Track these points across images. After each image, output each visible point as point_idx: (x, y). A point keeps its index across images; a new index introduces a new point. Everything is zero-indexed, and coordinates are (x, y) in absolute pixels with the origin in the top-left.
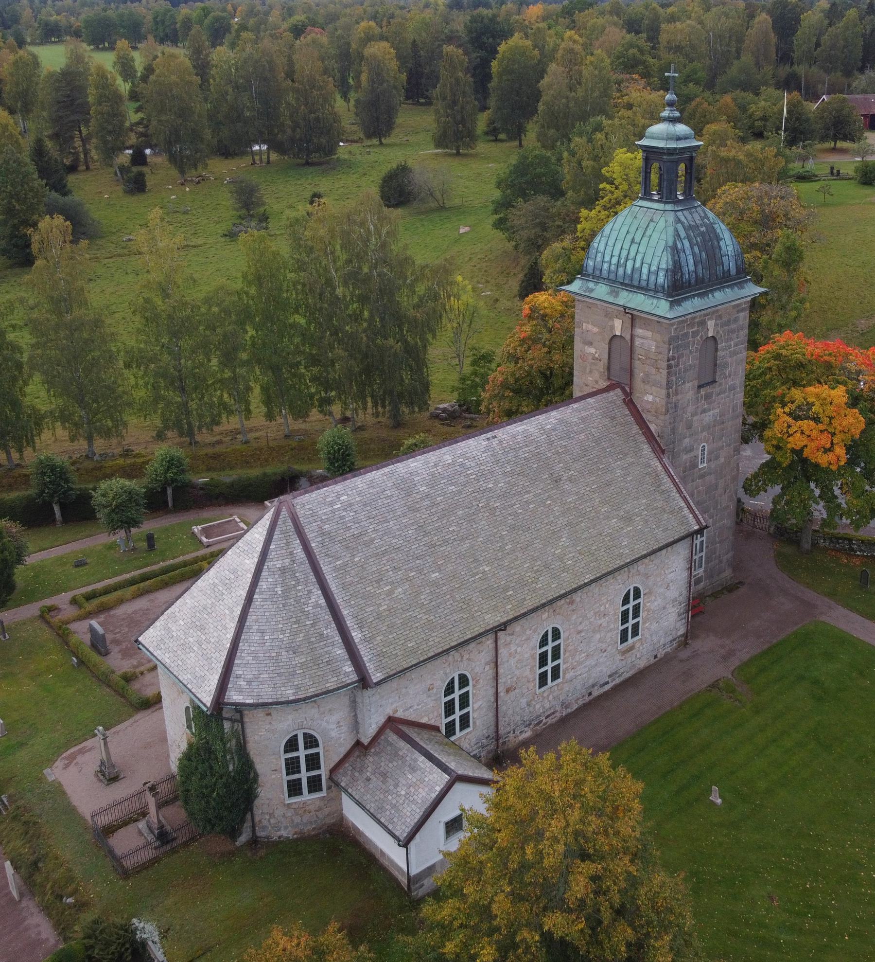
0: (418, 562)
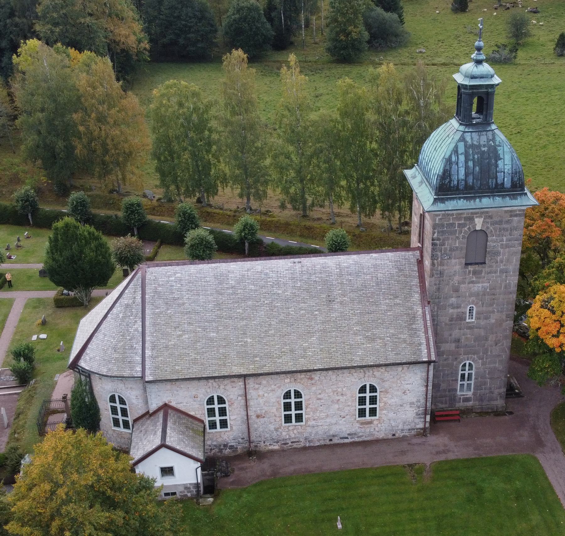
0: (206, 324)
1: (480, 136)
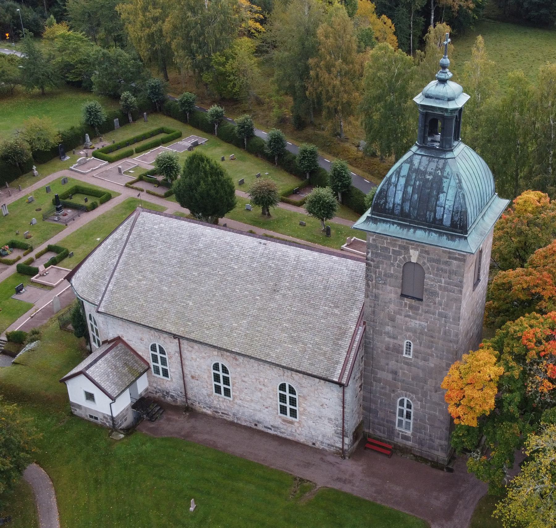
1: (429, 162)
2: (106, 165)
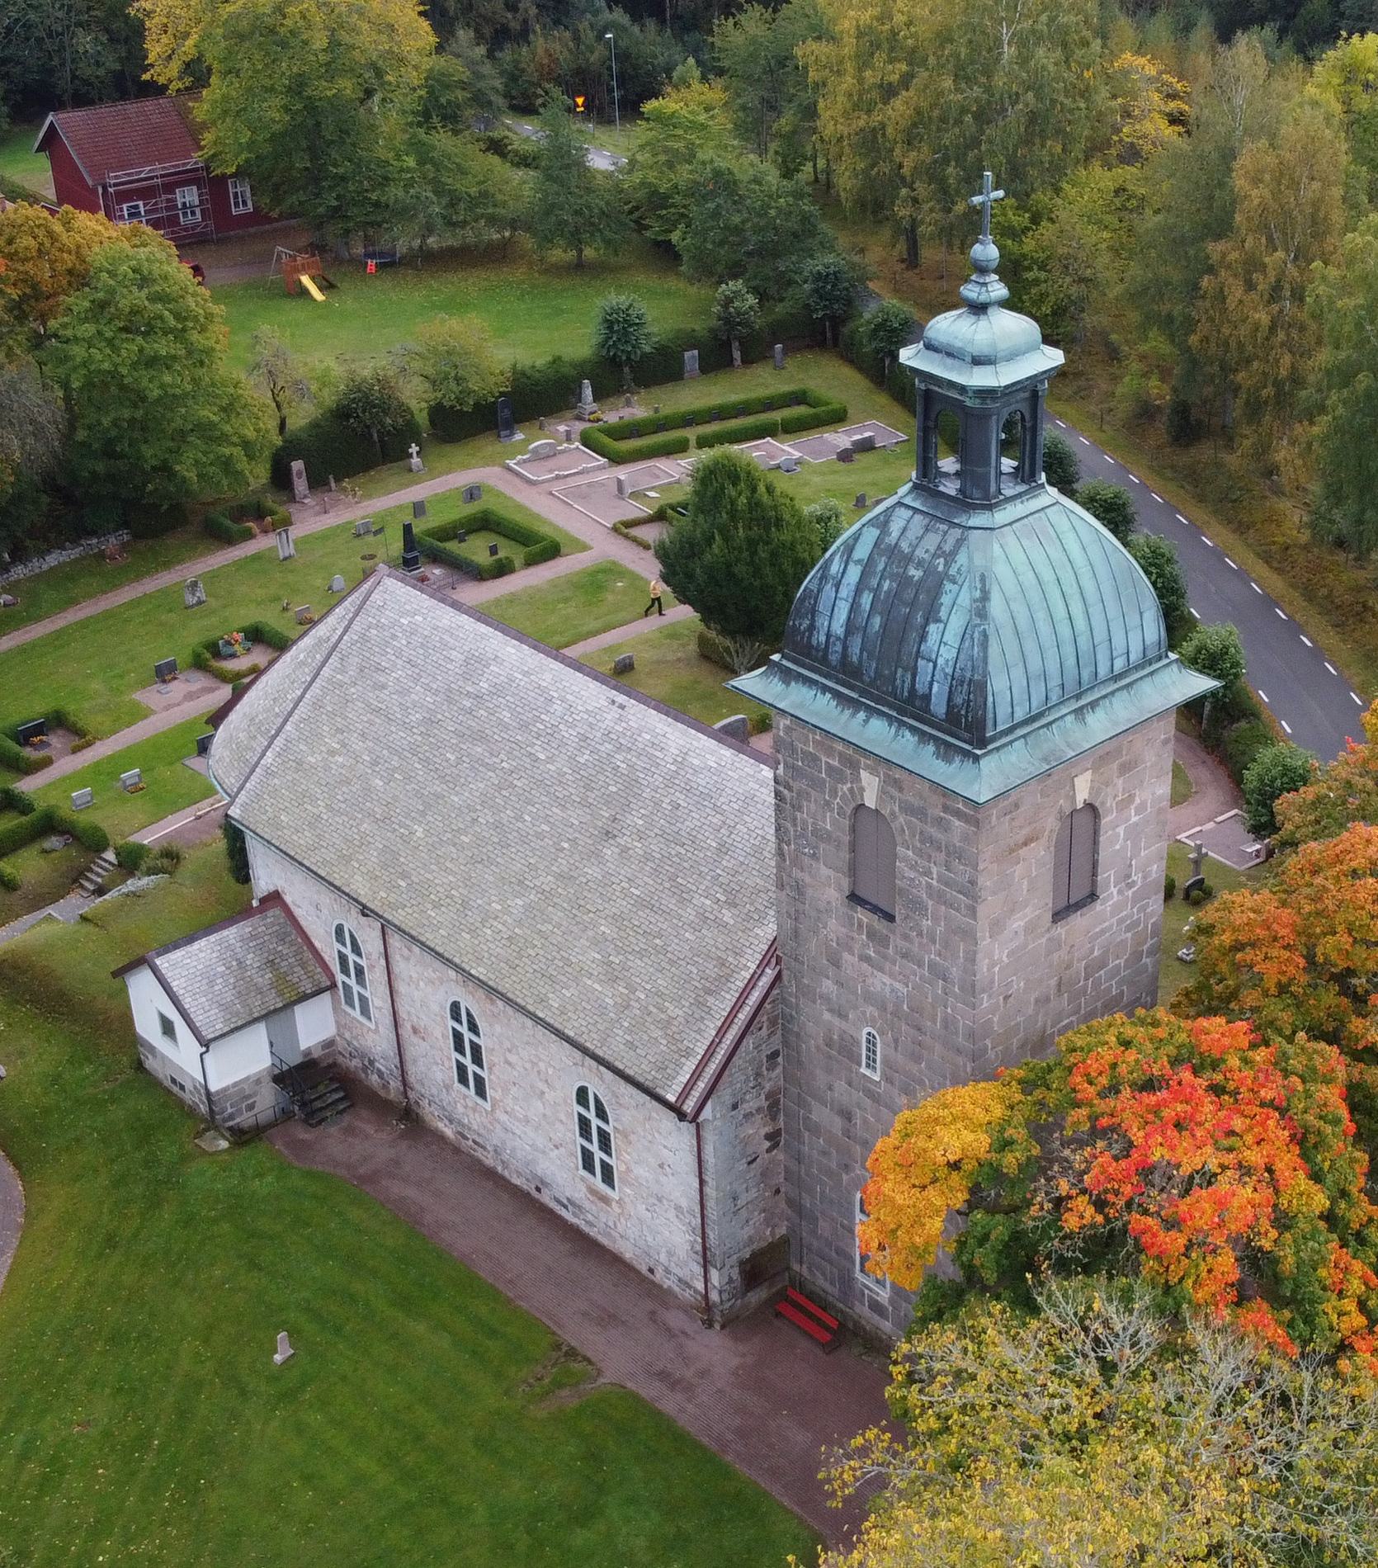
2: (600, 468)
